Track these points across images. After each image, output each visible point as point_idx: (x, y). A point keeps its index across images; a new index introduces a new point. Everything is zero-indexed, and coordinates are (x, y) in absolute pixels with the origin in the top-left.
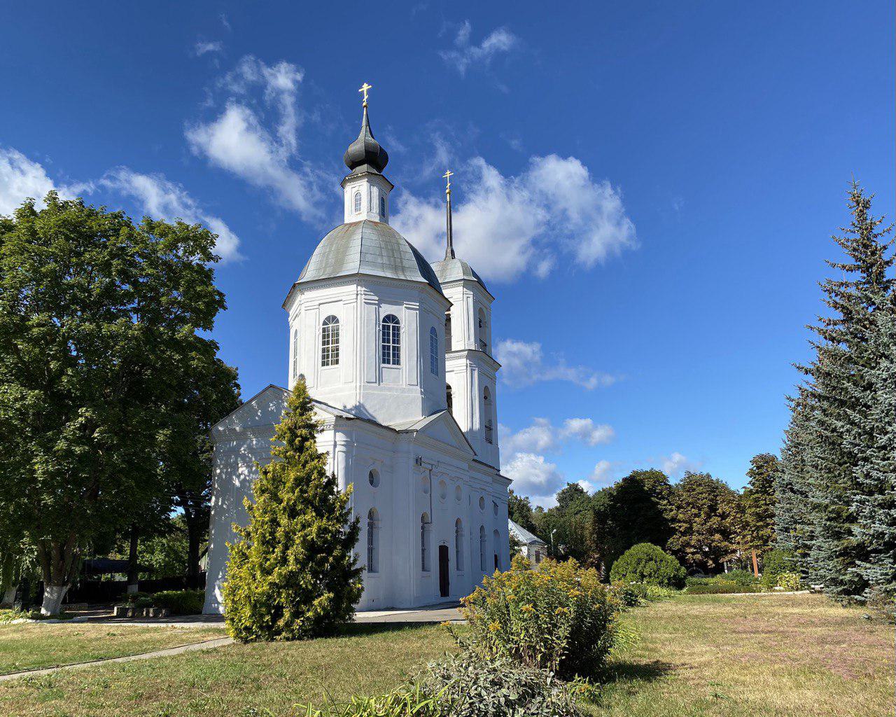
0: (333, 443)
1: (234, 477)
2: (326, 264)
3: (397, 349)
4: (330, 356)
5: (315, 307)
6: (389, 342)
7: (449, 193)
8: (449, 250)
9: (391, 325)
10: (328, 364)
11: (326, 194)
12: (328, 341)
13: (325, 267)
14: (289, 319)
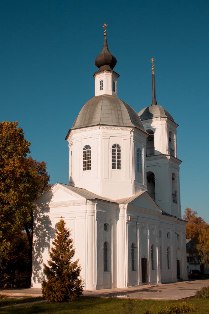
0: (85, 212)
1: (55, 249)
2: (85, 119)
3: (119, 161)
4: (87, 166)
5: (80, 141)
6: (115, 158)
7: (154, 70)
8: (154, 101)
9: (116, 149)
10: (86, 170)
11: (66, 231)
12: (86, 158)
13: (84, 121)
14: (69, 145)
